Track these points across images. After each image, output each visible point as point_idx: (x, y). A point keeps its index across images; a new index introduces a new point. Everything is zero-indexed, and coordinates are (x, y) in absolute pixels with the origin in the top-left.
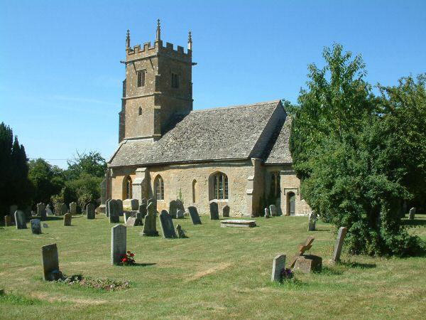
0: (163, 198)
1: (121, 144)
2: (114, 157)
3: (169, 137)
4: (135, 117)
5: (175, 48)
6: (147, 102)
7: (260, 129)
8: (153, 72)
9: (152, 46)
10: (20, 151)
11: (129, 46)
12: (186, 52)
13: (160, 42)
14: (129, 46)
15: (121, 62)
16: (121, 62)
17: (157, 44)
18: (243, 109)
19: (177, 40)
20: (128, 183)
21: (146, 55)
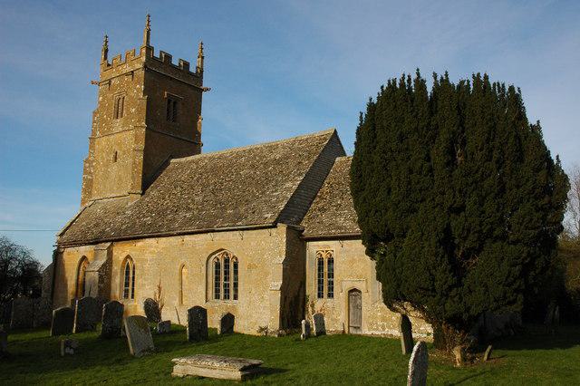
0: (331, 295)
1: (83, 207)
2: (68, 228)
3: (153, 192)
4: (107, 166)
5: (175, 62)
6: (128, 138)
7: (300, 175)
8: (137, 91)
9: (138, 55)
10: (378, 268)
11: (106, 58)
12: (192, 69)
13: (149, 49)
14: (106, 58)
15: (418, 70)
16: (418, 70)
17: (144, 51)
18: (272, 148)
19: (181, 51)
20: (128, 266)
21: (127, 69)
